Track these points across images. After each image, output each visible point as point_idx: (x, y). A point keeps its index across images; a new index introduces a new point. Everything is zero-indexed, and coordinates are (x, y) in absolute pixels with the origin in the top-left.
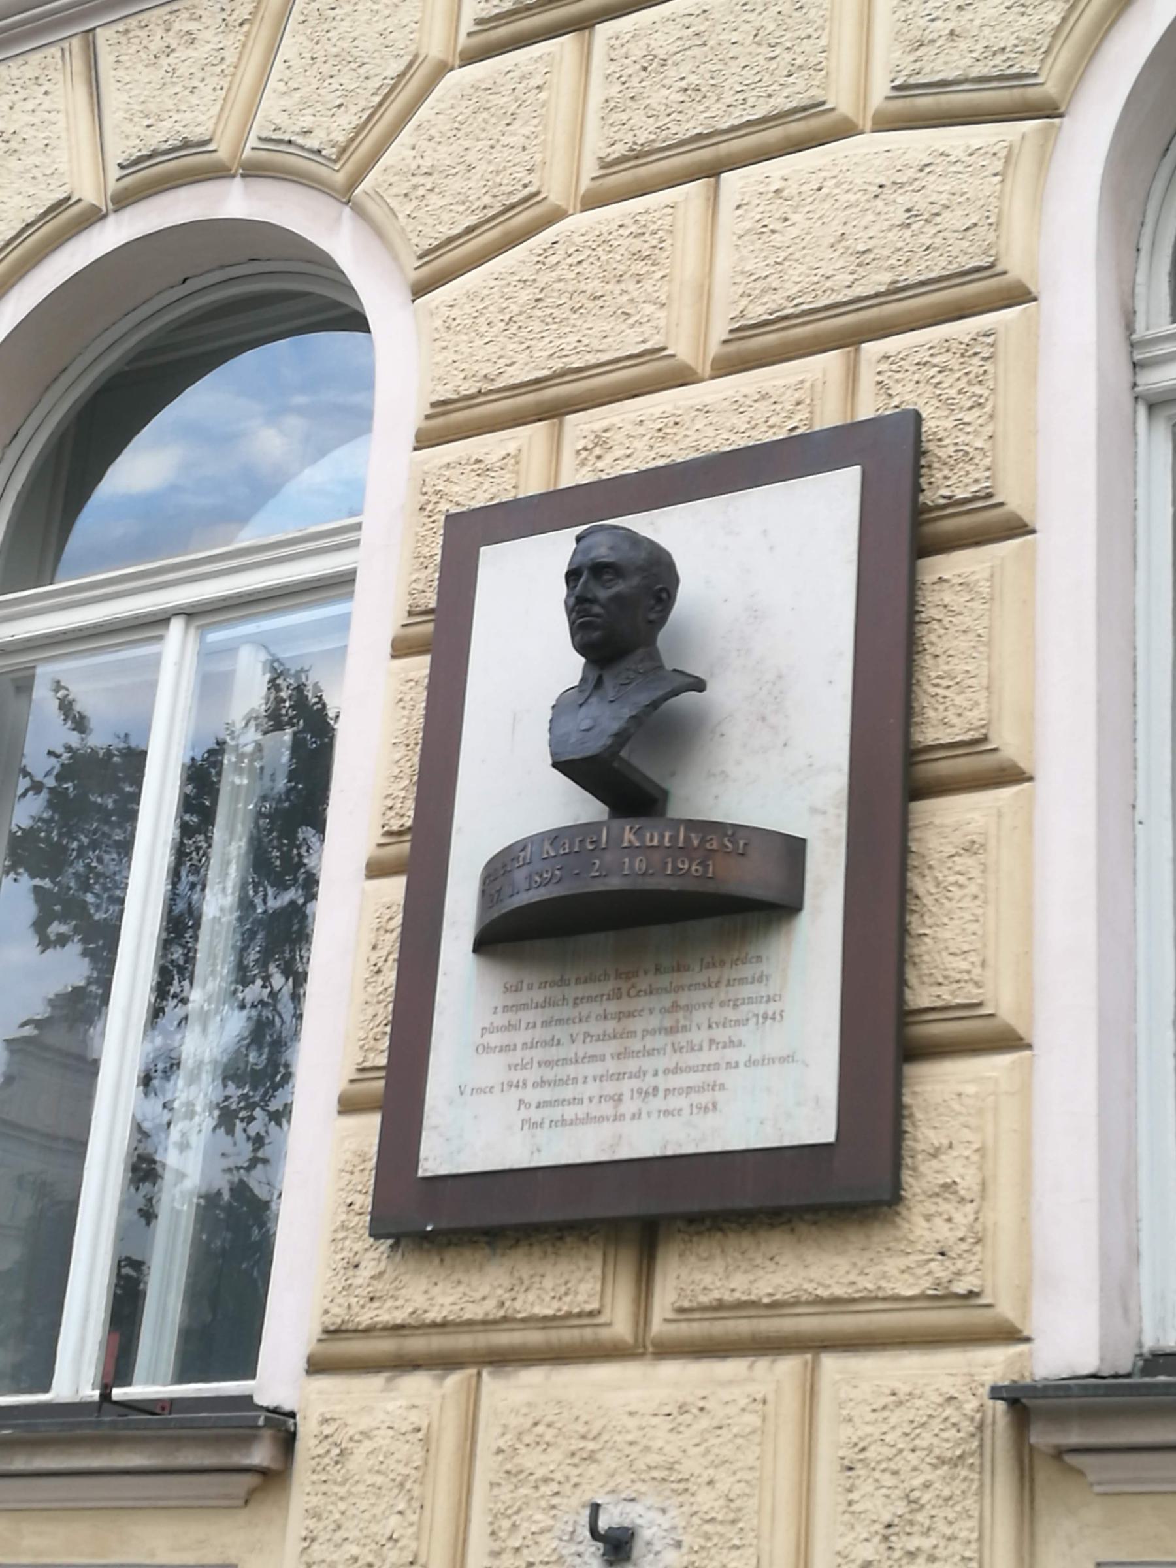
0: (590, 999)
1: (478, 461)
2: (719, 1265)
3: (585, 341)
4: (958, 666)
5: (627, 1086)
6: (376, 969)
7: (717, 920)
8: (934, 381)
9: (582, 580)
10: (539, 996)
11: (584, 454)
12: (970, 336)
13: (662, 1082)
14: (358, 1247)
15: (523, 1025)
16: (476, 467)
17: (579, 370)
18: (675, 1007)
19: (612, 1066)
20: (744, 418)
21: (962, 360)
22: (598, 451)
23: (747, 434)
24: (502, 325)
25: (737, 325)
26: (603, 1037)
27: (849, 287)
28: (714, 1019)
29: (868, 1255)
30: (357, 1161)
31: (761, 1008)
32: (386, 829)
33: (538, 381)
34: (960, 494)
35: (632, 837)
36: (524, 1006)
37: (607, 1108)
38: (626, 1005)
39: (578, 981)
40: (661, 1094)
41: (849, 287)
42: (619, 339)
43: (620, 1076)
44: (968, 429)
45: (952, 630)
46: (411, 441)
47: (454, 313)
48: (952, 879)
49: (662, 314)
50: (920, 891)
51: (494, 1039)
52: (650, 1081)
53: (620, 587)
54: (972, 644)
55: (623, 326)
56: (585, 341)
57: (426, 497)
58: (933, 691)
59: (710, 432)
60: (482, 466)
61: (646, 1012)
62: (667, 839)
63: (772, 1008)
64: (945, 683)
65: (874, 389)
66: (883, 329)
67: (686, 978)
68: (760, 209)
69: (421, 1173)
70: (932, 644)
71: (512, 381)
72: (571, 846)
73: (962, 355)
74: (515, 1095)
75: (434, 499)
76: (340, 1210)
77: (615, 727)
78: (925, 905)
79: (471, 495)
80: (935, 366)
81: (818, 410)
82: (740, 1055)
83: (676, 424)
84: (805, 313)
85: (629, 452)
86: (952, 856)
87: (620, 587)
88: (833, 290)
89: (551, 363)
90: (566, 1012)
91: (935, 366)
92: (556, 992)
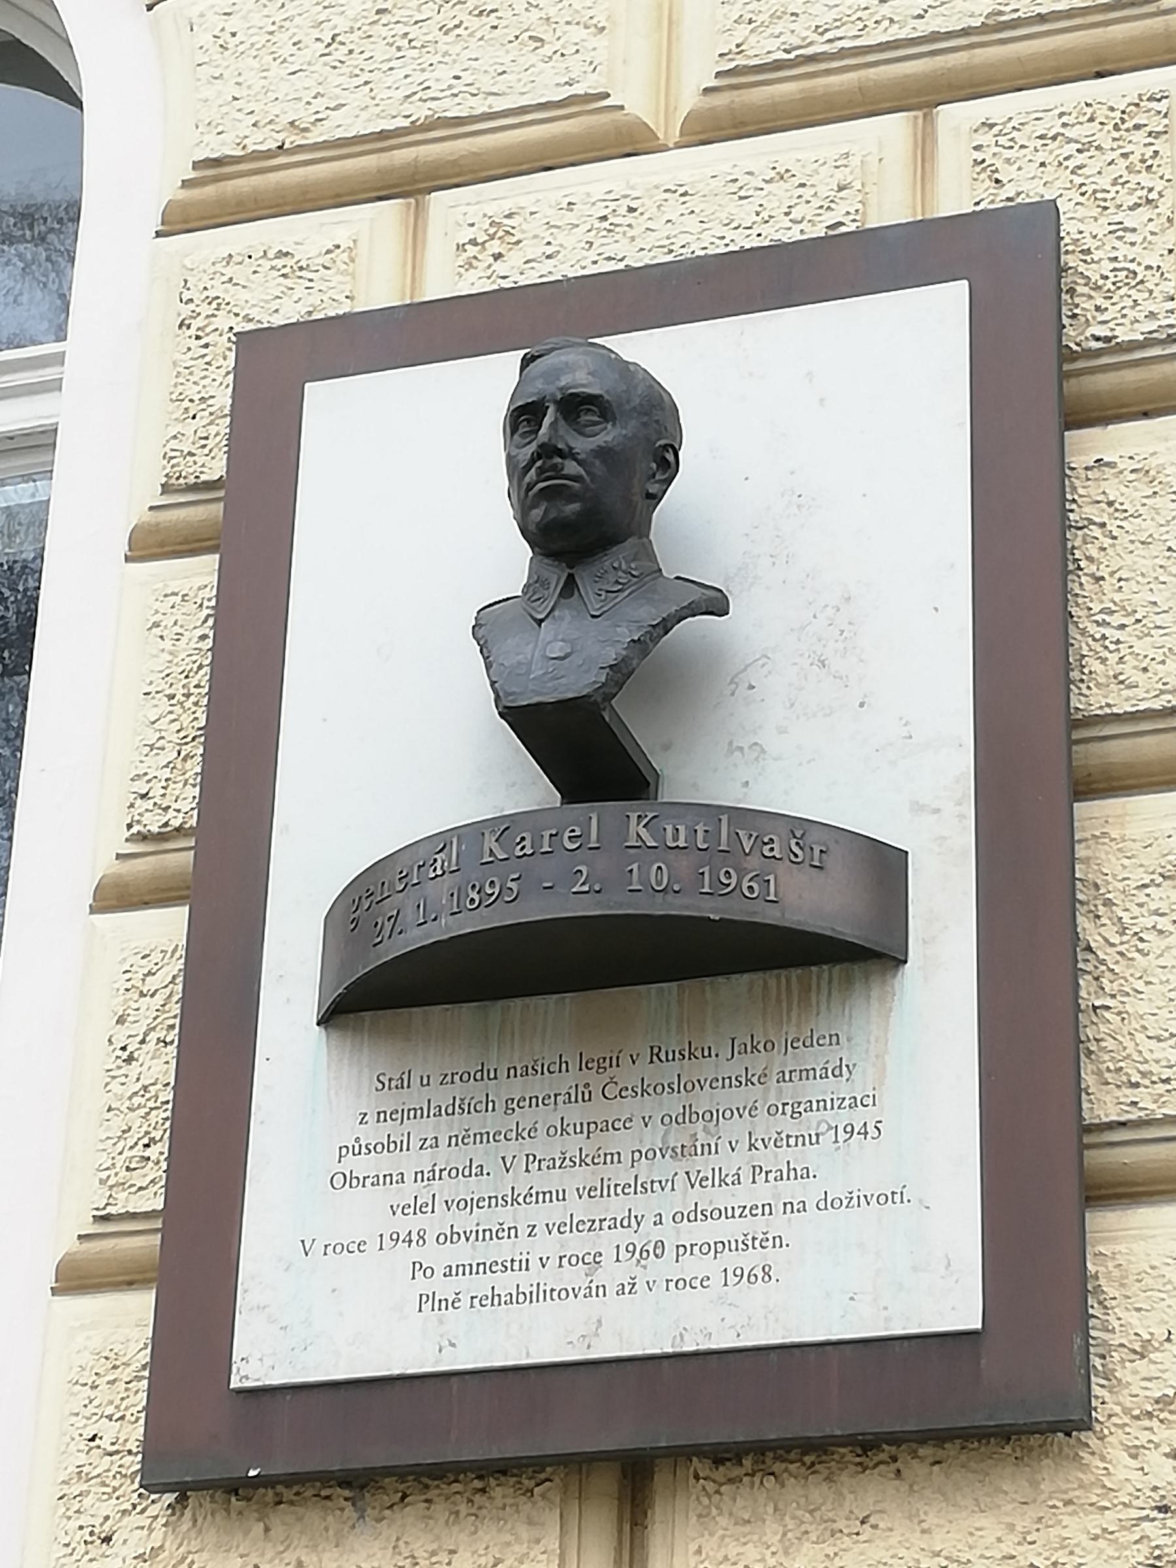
0: (534, 1101)
1: (282, 254)
2: (772, 1532)
3: (467, 77)
4: (1137, 596)
5: (607, 1241)
6: (125, 1055)
7: (757, 977)
8: (1071, 164)
9: (547, 421)
10: (442, 1096)
11: (472, 250)
12: (1128, 100)
13: (669, 1234)
14: (109, 1507)
15: (415, 1143)
16: (279, 263)
17: (459, 121)
18: (688, 1114)
19: (580, 1209)
20: (751, 206)
21: (1116, 135)
22: (495, 247)
23: (754, 232)
24: (320, 47)
25: (732, 65)
26: (564, 1162)
27: (920, 17)
28: (758, 1135)
29: (1032, 1513)
30: (102, 1366)
31: (842, 1118)
32: (134, 830)
33: (383, 135)
34: (1124, 335)
35: (643, 833)
36: (417, 1113)
37: (574, 1277)
38: (599, 1110)
39: (512, 1071)
40: (669, 1252)
41: (920, 17)
42: (526, 77)
43: (594, 1225)
44: (1130, 237)
45: (1124, 539)
46: (156, 224)
47: (232, 24)
48: (1149, 922)
49: (601, 41)
50: (1095, 941)
51: (362, 1165)
52: (650, 1233)
53: (608, 435)
54: (1159, 561)
55: (533, 59)
56: (467, 77)
57: (191, 306)
58: (1098, 632)
59: (692, 223)
60: (289, 262)
61: (637, 1122)
62: (700, 835)
63: (859, 1117)
64: (1116, 620)
65: (968, 170)
66: (972, 86)
67: (706, 1069)
68: (393, 33)
69: (235, 1384)
70: (1090, 559)
71: (339, 134)
72: (537, 842)
73: (1116, 127)
74: (406, 1255)
75: (206, 310)
76: (73, 1447)
77: (611, 655)
78: (1103, 962)
79: (274, 305)
80: (1070, 141)
81: (873, 199)
82: (811, 1192)
83: (631, 210)
84: (842, 53)
85: (549, 250)
86: (1145, 886)
87: (608, 435)
88: (892, 21)
89: (407, 108)
90: (492, 1122)
91: (1070, 141)
92: (475, 1090)
